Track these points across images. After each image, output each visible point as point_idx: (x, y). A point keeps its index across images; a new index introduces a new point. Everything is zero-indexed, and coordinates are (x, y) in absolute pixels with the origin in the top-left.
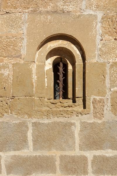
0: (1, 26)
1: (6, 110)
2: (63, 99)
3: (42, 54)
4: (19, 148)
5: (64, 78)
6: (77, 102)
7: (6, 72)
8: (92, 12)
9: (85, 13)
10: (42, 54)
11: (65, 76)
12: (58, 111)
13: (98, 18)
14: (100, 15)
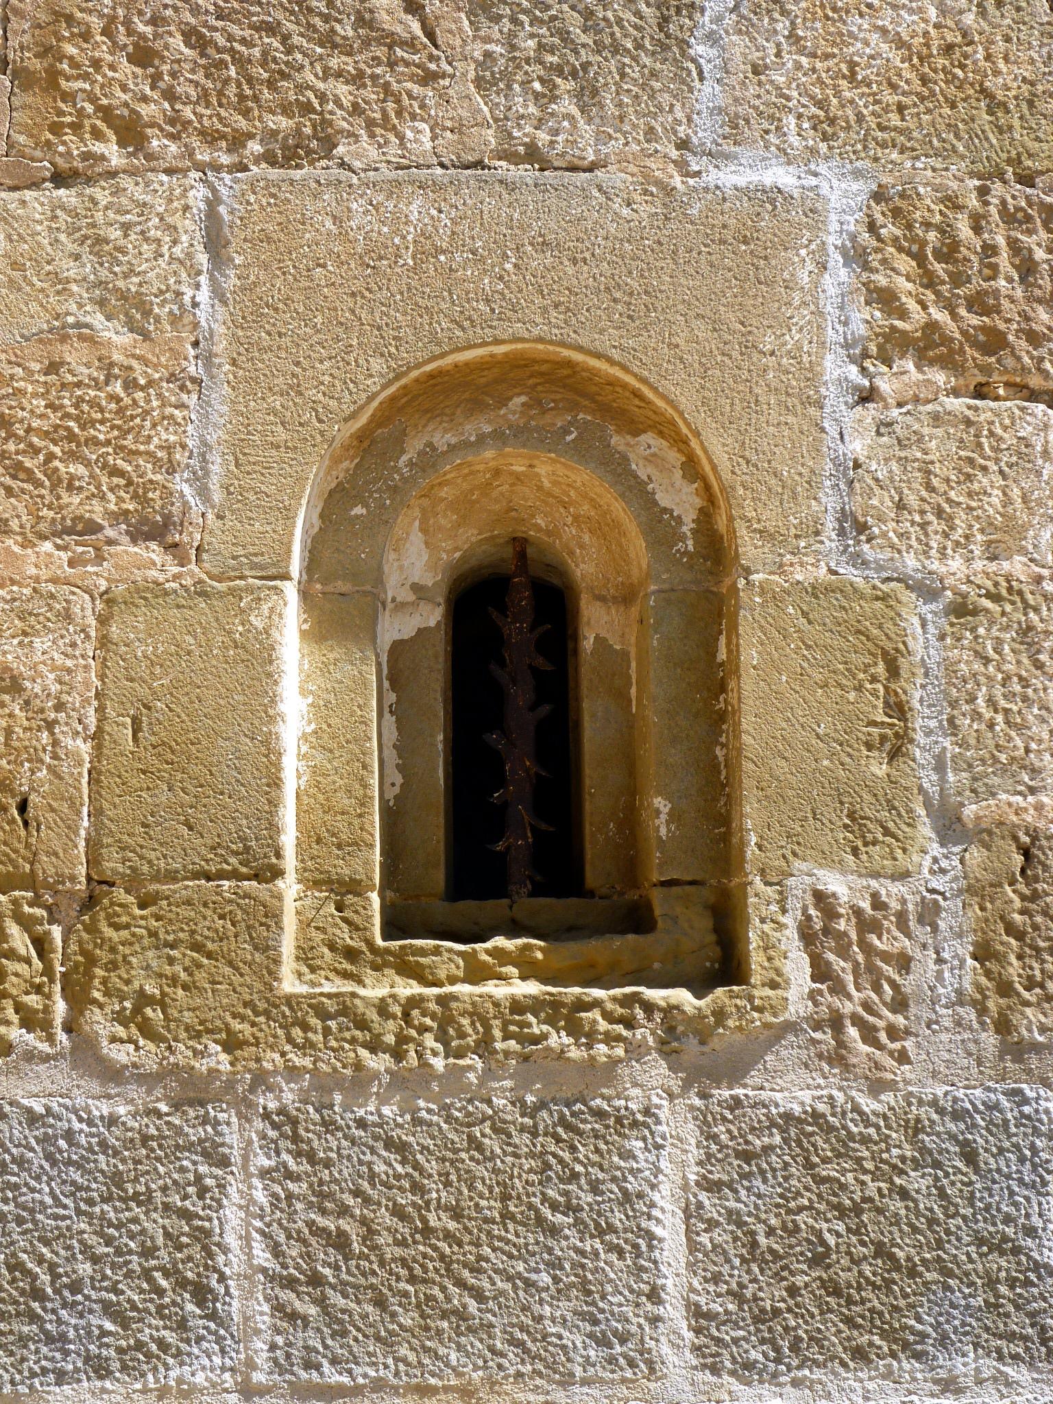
0: (1050, 503)
1: (33, 1000)
2: (533, 894)
3: (359, 510)
4: (139, 1346)
5: (545, 709)
6: (660, 924)
7: (45, 659)
8: (782, 176)
9: (729, 177)
10: (359, 510)
11: (542, 776)
12: (496, 1004)
13: (833, 217)
14: (842, 195)
